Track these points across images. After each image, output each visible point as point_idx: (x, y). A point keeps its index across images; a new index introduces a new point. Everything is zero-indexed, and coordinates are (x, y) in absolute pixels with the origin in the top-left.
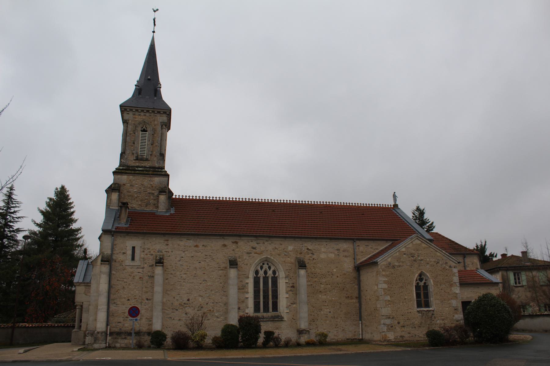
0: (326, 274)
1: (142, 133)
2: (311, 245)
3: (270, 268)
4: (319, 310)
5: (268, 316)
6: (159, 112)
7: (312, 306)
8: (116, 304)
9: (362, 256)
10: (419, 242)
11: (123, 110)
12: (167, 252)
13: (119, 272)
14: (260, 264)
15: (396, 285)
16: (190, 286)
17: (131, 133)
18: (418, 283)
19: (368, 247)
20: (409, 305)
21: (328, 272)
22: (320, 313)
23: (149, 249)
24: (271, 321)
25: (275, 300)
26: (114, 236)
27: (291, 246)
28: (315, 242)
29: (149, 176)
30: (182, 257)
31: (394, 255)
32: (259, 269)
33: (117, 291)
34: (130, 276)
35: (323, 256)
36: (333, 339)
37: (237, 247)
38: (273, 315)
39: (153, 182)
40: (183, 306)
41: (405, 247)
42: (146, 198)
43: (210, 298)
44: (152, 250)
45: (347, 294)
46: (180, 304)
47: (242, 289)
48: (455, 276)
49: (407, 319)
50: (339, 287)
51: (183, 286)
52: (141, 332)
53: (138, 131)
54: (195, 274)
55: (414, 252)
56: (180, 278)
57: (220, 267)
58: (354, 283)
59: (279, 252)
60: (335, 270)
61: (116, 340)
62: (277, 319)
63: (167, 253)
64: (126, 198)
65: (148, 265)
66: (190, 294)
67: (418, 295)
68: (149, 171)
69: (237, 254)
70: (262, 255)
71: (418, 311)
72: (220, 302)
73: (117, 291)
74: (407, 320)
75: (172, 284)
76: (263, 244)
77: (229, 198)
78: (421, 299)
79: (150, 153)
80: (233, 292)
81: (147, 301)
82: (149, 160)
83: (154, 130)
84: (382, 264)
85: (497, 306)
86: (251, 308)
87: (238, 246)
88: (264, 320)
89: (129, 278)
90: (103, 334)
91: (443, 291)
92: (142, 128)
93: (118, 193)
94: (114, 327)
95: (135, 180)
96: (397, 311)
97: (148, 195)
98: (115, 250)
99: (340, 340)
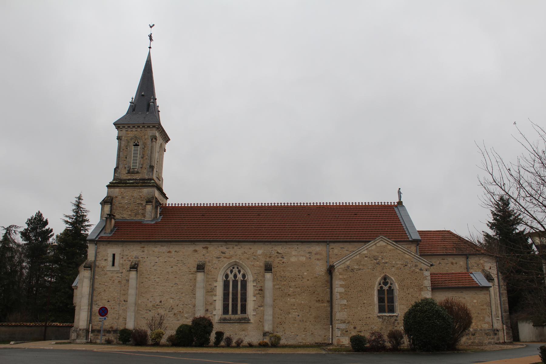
0: (296, 278)
1: (134, 148)
2: (281, 248)
3: (239, 272)
4: (287, 313)
5: (236, 318)
6: (149, 127)
7: (280, 309)
8: (98, 305)
9: (336, 258)
10: (384, 244)
12: (143, 258)
13: (101, 276)
14: (229, 268)
15: (354, 289)
16: (162, 289)
17: (124, 148)
18: (381, 287)
19: (343, 249)
20: (368, 310)
21: (298, 275)
22: (287, 316)
23: (127, 255)
24: (237, 323)
25: (244, 303)
26: (97, 245)
27: (260, 250)
28: (286, 245)
29: (138, 187)
30: (156, 263)
31: (354, 258)
32: (229, 273)
33: (99, 294)
34: (110, 280)
35: (293, 259)
36: (301, 343)
37: (207, 252)
38: (240, 317)
39: (142, 193)
40: (155, 307)
41: (367, 249)
42: (136, 208)
43: (180, 300)
44: (130, 256)
45: (317, 298)
46: (153, 306)
47: (210, 291)
48: (426, 279)
49: (365, 325)
50: (310, 291)
51: (156, 289)
52: (118, 330)
53: (130, 146)
54: (168, 278)
55: (377, 254)
56: (153, 281)
57: (190, 271)
58: (326, 286)
59: (247, 256)
60: (305, 274)
61: (97, 337)
62: (243, 321)
63: (143, 259)
64: (118, 209)
65: (125, 270)
66: (162, 296)
67: (381, 300)
68: (139, 183)
69: (207, 258)
70: (231, 259)
71: (379, 317)
72: (189, 304)
73: (99, 294)
74: (364, 326)
75: (147, 287)
76: (232, 248)
77: (372, 203)
78: (385, 303)
79: (141, 166)
80: (200, 294)
81: (124, 302)
82: (140, 173)
83: (145, 144)
84: (339, 267)
85: (429, 313)
86: (219, 309)
87: (208, 251)
88: (231, 322)
89: (109, 282)
90: (84, 331)
91: (410, 296)
92: (134, 142)
94: (96, 325)
95: (126, 192)
96: (354, 316)
97: (137, 205)
98: (98, 257)
99: (308, 344)
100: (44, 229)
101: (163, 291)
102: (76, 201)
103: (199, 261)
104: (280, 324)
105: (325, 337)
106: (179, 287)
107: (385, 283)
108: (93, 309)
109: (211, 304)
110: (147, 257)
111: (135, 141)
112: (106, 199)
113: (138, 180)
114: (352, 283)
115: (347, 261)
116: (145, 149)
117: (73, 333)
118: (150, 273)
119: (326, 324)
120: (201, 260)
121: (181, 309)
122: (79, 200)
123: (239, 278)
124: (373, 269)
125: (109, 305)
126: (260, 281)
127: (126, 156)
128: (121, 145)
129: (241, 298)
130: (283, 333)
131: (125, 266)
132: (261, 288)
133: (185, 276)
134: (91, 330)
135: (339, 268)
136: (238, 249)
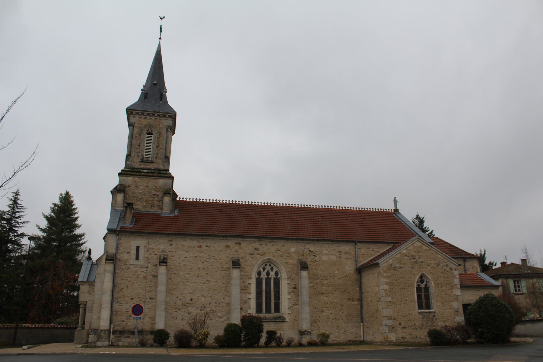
1: (147, 136)
2: (313, 247)
5: (271, 317)
6: (164, 116)
7: (314, 307)
10: (420, 244)
11: (129, 113)
12: (171, 252)
14: (262, 265)
15: (397, 287)
18: (419, 285)
19: (369, 250)
21: (330, 274)
23: (153, 249)
24: (273, 322)
25: (277, 301)
27: (293, 248)
28: (317, 244)
29: (154, 177)
30: (186, 257)
31: (395, 257)
32: (262, 270)
33: (121, 290)
35: (325, 258)
36: (334, 341)
37: (240, 248)
38: (275, 316)
39: (158, 184)
40: (185, 306)
41: (406, 248)
42: (151, 199)
43: (212, 299)
44: (156, 250)
46: (183, 304)
47: (244, 289)
48: (456, 278)
50: (341, 289)
51: (186, 286)
52: (144, 331)
54: (199, 274)
55: (415, 254)
58: (356, 285)
59: (281, 253)
61: (119, 339)
62: (279, 320)
63: (171, 253)
65: (151, 265)
69: (240, 255)
70: (264, 256)
71: (419, 313)
72: (222, 302)
73: (121, 290)
76: (265, 245)
79: (155, 155)
80: (235, 291)
82: (154, 163)
83: (160, 134)
86: (254, 308)
88: (267, 321)
90: (107, 332)
91: (444, 293)
92: (148, 131)
93: (123, 194)
94: (117, 326)
95: (140, 182)
96: (398, 312)
99: (342, 341)
100: (54, 216)
101: (194, 289)
102: (13, 196)
103: (233, 257)
104: (315, 322)
105: (356, 335)
106: (211, 284)
107: (422, 281)
108: (114, 308)
109: (245, 302)
110: (176, 252)
111: (148, 129)
112: (118, 187)
113: (152, 170)
114: (395, 281)
115: (389, 259)
116: (160, 138)
117: (91, 335)
118: (179, 268)
119: (357, 321)
120: (234, 256)
121: (214, 307)
122: (16, 195)
123: (273, 276)
124: (412, 268)
125: (133, 303)
126: (294, 279)
127: (140, 143)
128: (133, 132)
129: (274, 296)
130: (317, 331)
131: (150, 260)
132: (295, 286)
133: (217, 272)
134: (113, 331)
135: (383, 266)
136: (271, 246)
